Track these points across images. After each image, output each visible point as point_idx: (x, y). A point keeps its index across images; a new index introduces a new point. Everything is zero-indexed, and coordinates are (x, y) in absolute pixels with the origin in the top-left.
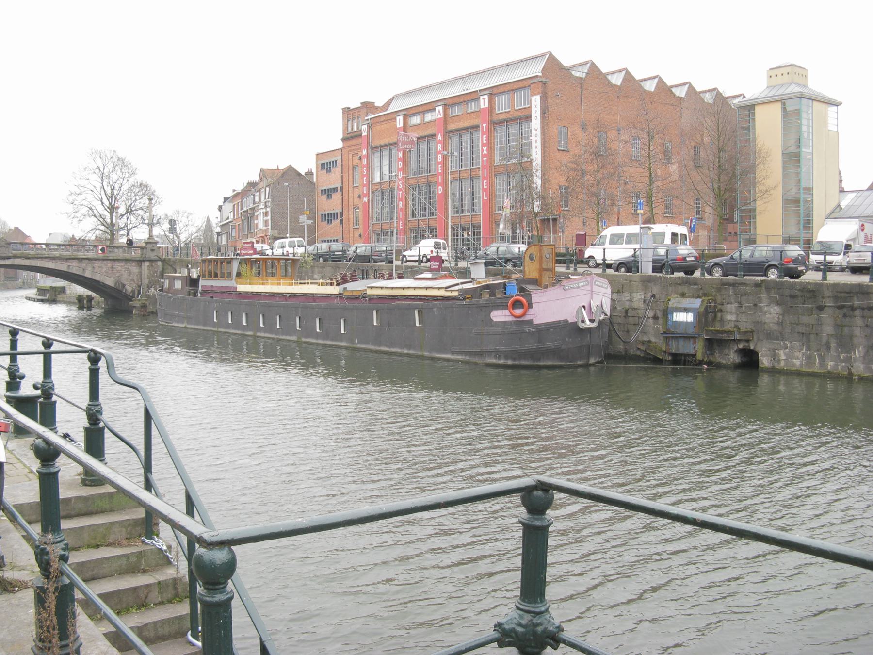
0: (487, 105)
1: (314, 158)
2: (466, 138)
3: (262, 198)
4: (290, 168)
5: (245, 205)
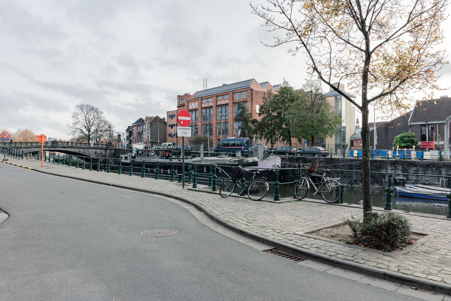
1: (166, 113)
2: (208, 110)
3: (146, 127)
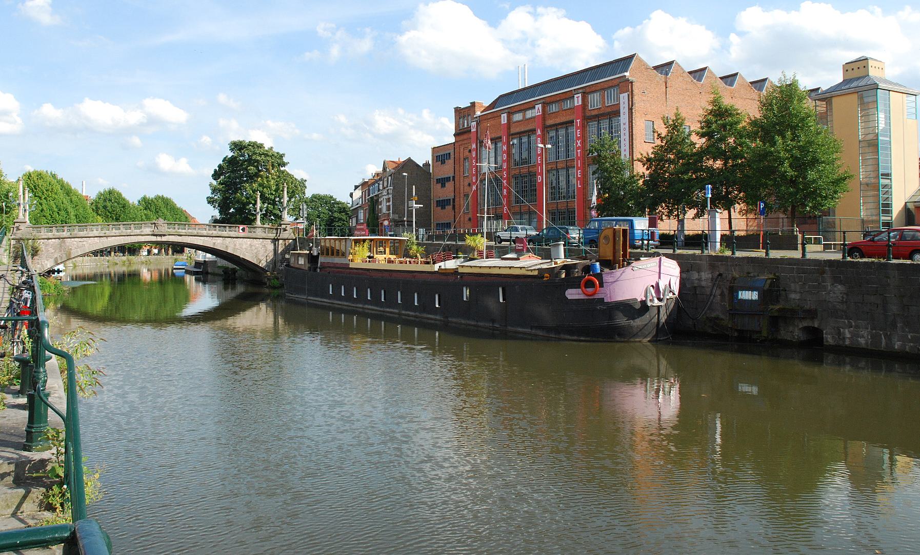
0: (580, 103)
4: (409, 161)
5: (371, 192)
